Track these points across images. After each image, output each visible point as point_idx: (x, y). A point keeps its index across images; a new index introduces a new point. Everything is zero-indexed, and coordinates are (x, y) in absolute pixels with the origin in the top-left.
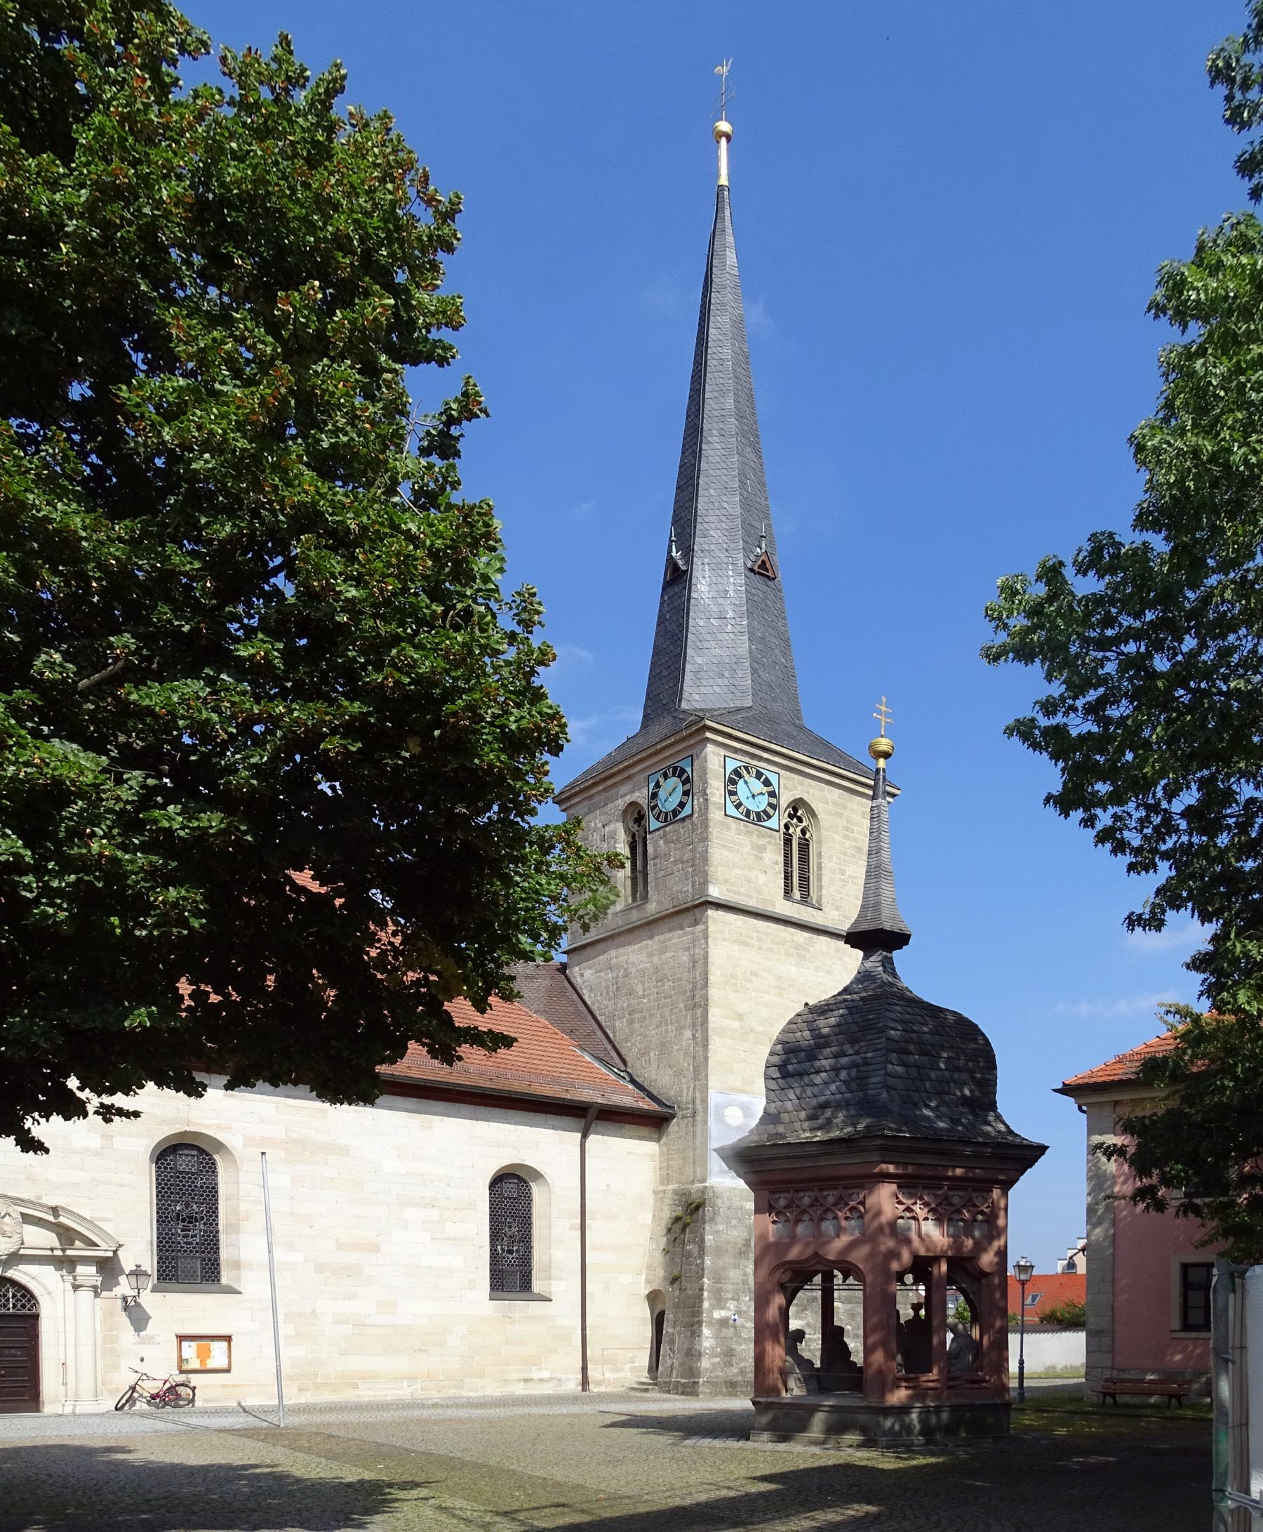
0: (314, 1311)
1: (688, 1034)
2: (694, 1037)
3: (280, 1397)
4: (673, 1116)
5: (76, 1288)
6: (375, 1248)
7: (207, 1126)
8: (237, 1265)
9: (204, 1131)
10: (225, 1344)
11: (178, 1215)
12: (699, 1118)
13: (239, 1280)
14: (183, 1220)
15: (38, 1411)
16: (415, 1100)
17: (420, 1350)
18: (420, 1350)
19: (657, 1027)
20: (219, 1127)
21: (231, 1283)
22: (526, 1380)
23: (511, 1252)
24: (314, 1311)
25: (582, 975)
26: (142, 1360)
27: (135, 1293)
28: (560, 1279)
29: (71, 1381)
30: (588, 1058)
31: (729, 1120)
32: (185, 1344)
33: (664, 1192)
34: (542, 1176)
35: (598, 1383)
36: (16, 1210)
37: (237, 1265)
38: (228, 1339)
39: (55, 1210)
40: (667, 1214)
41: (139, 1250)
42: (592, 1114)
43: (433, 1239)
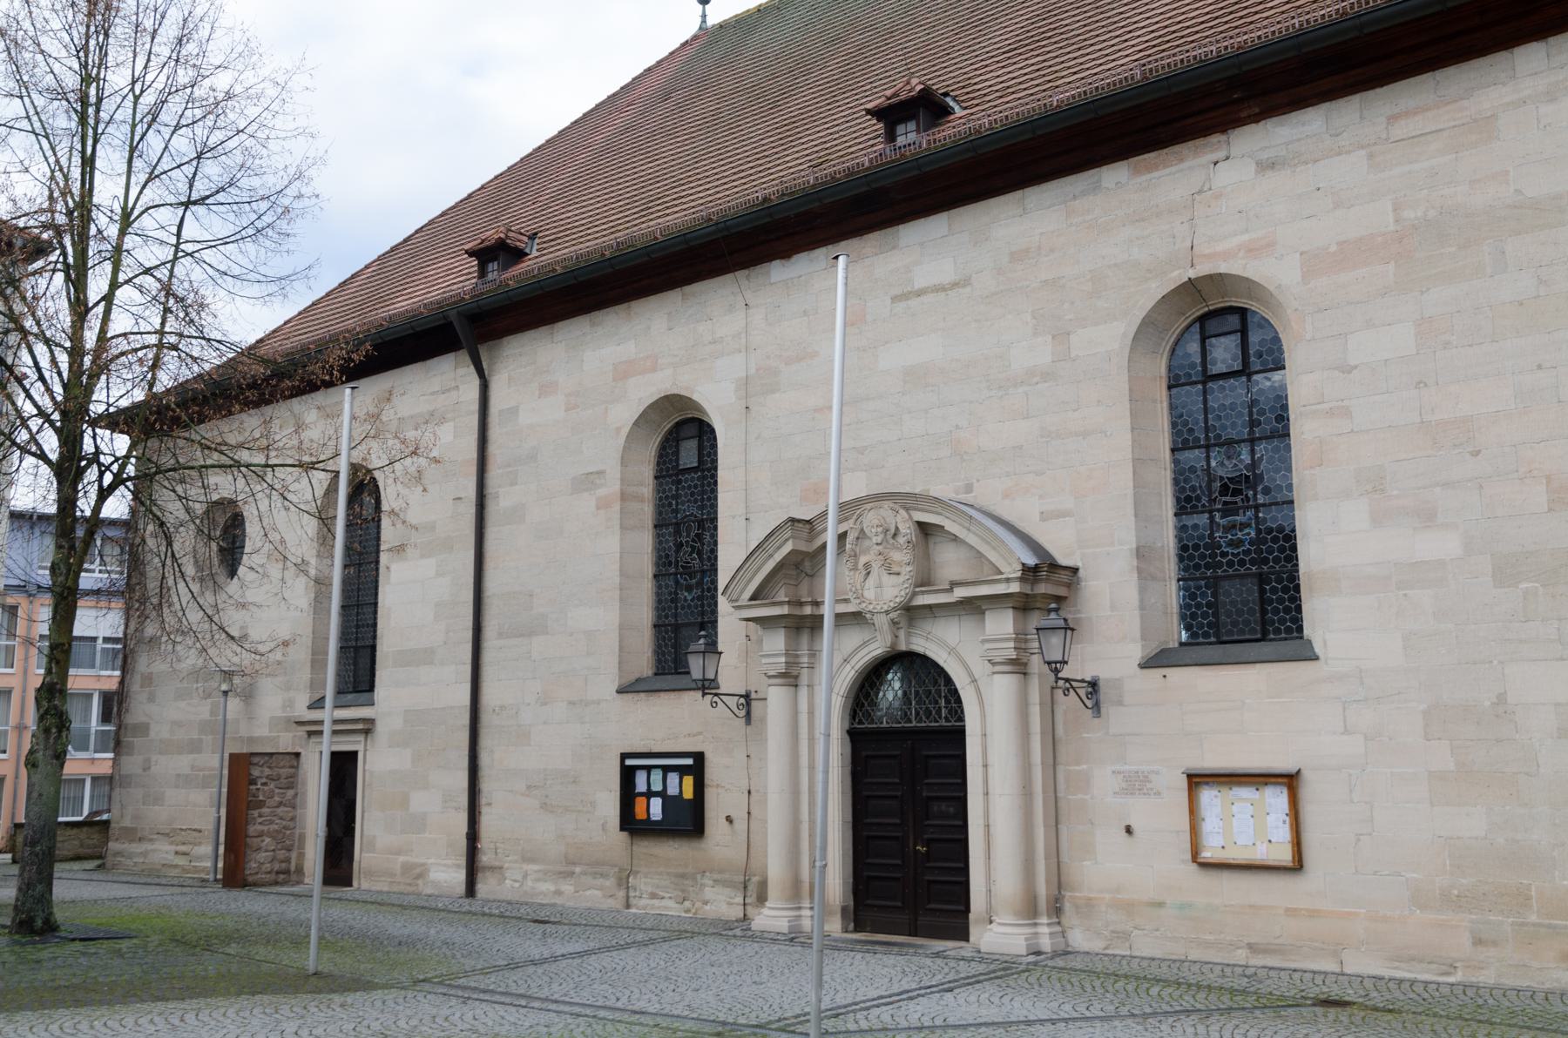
0: (1501, 698)
9: (1223, 268)
20: (1252, 250)
24: (1501, 698)
32: (1209, 797)
38: (1290, 781)
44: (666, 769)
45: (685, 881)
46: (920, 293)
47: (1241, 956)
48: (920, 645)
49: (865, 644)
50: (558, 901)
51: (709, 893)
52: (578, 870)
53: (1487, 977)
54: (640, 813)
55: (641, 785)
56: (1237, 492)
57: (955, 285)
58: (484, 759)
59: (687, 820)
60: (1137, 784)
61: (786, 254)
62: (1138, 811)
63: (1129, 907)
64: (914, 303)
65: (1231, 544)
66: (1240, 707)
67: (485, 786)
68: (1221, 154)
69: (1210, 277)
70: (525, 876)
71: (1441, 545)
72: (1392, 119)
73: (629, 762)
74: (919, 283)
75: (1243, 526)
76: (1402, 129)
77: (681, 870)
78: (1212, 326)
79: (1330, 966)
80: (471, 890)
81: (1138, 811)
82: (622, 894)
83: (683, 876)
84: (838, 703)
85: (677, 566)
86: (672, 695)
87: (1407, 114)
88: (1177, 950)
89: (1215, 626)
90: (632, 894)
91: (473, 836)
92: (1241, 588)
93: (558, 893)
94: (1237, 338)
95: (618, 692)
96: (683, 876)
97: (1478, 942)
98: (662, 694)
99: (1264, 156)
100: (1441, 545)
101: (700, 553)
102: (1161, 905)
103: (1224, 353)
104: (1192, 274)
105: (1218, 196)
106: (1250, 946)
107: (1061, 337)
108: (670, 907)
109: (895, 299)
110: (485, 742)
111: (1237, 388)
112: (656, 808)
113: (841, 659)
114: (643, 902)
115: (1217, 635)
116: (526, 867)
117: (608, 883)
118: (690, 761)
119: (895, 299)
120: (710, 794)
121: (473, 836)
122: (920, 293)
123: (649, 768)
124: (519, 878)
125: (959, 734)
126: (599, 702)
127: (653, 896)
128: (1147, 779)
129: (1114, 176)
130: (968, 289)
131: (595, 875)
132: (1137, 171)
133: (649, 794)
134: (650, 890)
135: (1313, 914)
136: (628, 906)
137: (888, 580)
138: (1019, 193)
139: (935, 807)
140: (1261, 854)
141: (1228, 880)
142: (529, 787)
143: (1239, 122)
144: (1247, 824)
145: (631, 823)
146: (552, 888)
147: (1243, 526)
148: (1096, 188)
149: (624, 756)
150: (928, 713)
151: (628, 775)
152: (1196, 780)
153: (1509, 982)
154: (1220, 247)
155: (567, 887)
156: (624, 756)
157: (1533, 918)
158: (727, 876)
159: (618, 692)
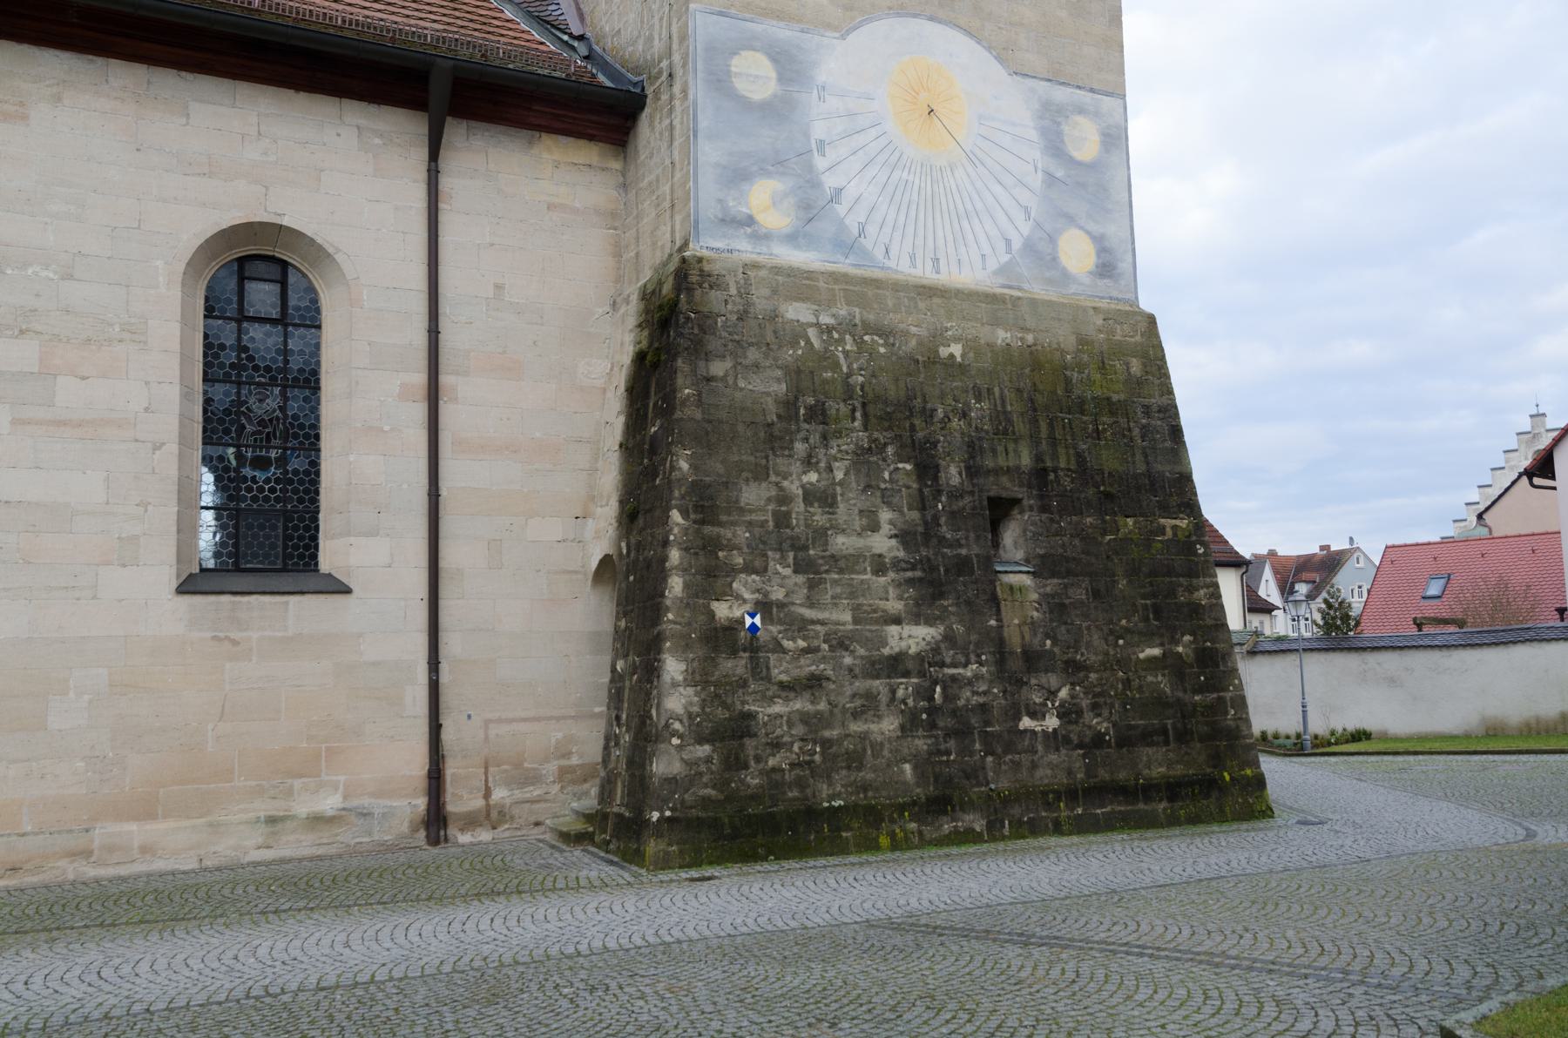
12: (677, 89)
22: (272, 820)
23: (261, 463)
28: (373, 533)
31: (741, 86)
35: (491, 817)
43: (15, 422)
78: (250, 269)
94: (276, 288)
103: (262, 296)
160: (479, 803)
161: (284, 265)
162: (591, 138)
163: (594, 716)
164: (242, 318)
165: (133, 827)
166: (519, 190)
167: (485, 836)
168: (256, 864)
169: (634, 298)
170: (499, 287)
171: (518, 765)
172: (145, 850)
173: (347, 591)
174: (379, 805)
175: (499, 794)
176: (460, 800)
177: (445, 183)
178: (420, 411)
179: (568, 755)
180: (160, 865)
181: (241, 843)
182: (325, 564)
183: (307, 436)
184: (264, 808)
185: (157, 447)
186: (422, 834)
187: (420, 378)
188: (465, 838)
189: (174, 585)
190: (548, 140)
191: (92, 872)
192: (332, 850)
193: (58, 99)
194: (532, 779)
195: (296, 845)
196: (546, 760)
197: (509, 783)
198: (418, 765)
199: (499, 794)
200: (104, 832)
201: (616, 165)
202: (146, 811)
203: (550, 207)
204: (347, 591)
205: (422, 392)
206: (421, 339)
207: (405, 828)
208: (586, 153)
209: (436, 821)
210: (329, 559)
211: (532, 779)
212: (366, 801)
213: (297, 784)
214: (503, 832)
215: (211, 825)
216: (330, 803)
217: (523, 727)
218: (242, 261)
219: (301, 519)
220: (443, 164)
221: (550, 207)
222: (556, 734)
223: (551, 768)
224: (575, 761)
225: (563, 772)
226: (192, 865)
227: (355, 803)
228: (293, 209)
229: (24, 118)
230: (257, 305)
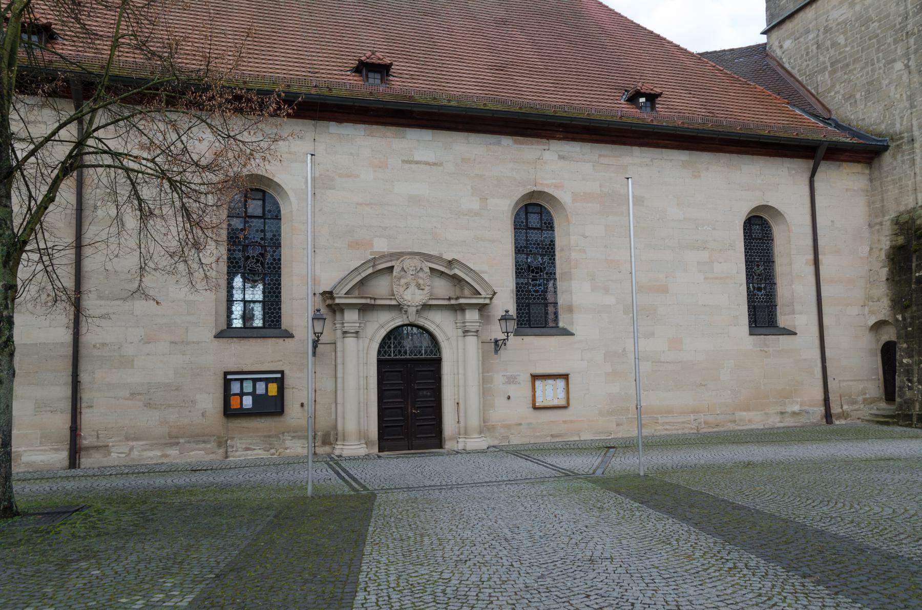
0: (624, 349)
1: (899, 66)
2: (907, 66)
3: (259, 302)
4: (886, 148)
5: (466, 332)
6: (664, 290)
7: (548, 186)
8: (570, 309)
9: (546, 190)
10: (561, 383)
11: (529, 266)
13: (572, 323)
14: (533, 272)
15: (441, 447)
16: (687, 152)
17: (701, 385)
18: (701, 385)
19: (862, 69)
20: (556, 186)
21: (566, 327)
22: (782, 413)
23: (759, 289)
24: (624, 349)
25: (781, 47)
26: (509, 398)
27: (504, 336)
28: (801, 313)
29: (462, 420)
30: (798, 112)
32: (538, 383)
33: (881, 224)
34: (781, 215)
35: (844, 415)
36: (427, 265)
37: (570, 309)
38: (565, 377)
39: (450, 263)
40: (885, 244)
41: (505, 302)
42: (821, 152)
43: (706, 279)
44: (255, 381)
45: (269, 440)
46: (417, 163)
47: (549, 439)
48: (421, 322)
49: (394, 319)
50: (165, 460)
51: (288, 443)
52: (182, 441)
53: (620, 435)
54: (235, 403)
55: (235, 388)
56: (537, 273)
57: (435, 164)
58: (84, 377)
59: (271, 407)
60: (511, 380)
61: (340, 121)
62: (512, 390)
63: (509, 427)
64: (414, 166)
65: (535, 291)
66: (540, 351)
67: (86, 395)
68: (546, 147)
69: (540, 192)
70: (131, 449)
71: (610, 300)
72: (600, 156)
73: (229, 377)
74: (417, 158)
75: (540, 285)
76: (604, 160)
77: (265, 434)
78: (530, 209)
79: (576, 438)
80: (73, 462)
81: (512, 390)
82: (222, 451)
83: (269, 436)
84: (375, 346)
85: (245, 268)
86: (259, 340)
87: (604, 156)
88: (526, 440)
89: (529, 321)
90: (230, 450)
91: (75, 430)
92: (536, 308)
93: (166, 456)
94: (260, 203)
95: (215, 337)
96: (269, 436)
97: (618, 425)
98: (251, 340)
99: (561, 153)
100: (610, 300)
101: (262, 264)
102: (520, 424)
103: (534, 220)
104: (535, 189)
105: (545, 163)
106: (552, 436)
107: (484, 199)
108: (259, 453)
109: (403, 161)
110: (84, 366)
111: (257, 223)
112: (248, 402)
113: (381, 325)
114: (238, 453)
115: (529, 324)
116: (131, 443)
117: (209, 446)
118: (279, 376)
119: (403, 161)
120: (288, 394)
121: (75, 430)
122: (417, 163)
123: (242, 380)
124: (127, 450)
125: (438, 361)
126: (198, 343)
127: (247, 449)
128: (515, 378)
129: (506, 141)
130: (441, 168)
131: (198, 442)
132: (516, 142)
133: (242, 394)
134: (244, 446)
135: (572, 422)
136: (227, 457)
137: (418, 292)
138: (466, 134)
139: (420, 393)
140: (556, 402)
141: (543, 413)
142: (132, 394)
143: (554, 138)
144: (550, 392)
145: (230, 412)
146: (159, 453)
147: (540, 285)
148: (499, 144)
149: (226, 374)
150: (400, 352)
151: (227, 383)
152: (535, 377)
153: (625, 436)
154: (546, 182)
155: (173, 452)
156: (226, 374)
157: (630, 416)
158: (300, 434)
159: (215, 337)
160: (840, 410)
161: (264, 192)
162: (859, 162)
163: (872, 380)
164: (528, 228)
165: (744, 413)
166: (842, 186)
167: (843, 422)
168: (778, 428)
169: (888, 223)
170: (832, 222)
171: (850, 397)
172: (750, 421)
173: (796, 334)
174: (811, 409)
175: (845, 407)
176: (835, 410)
177: (817, 185)
178: (812, 269)
179: (865, 394)
180: (753, 427)
181: (775, 421)
182: (561, 324)
183: (274, 268)
184: (779, 409)
185: (741, 285)
186: (824, 420)
187: (811, 257)
188: (837, 422)
189: (214, 333)
190: (845, 164)
191: (737, 428)
192: (799, 425)
193: (708, 169)
194: (854, 402)
195: (789, 422)
196: (858, 396)
197: (849, 403)
198: (820, 396)
199: (845, 407)
200: (740, 414)
201: (867, 172)
202: (747, 408)
203: (847, 190)
204: (796, 334)
205: (812, 262)
206: (810, 242)
207: (819, 418)
208: (857, 168)
209: (828, 416)
210: (783, 321)
211: (854, 402)
212: (806, 408)
213: (787, 401)
214: (848, 421)
215: (766, 414)
216: (796, 408)
217: (851, 383)
218: (527, 206)
219: (272, 305)
220: (816, 178)
221: (847, 190)
222: (861, 386)
223: (860, 398)
224: (867, 396)
225: (865, 400)
226: (762, 427)
227: (804, 408)
228: (772, 201)
229: (700, 176)
230: (535, 222)
